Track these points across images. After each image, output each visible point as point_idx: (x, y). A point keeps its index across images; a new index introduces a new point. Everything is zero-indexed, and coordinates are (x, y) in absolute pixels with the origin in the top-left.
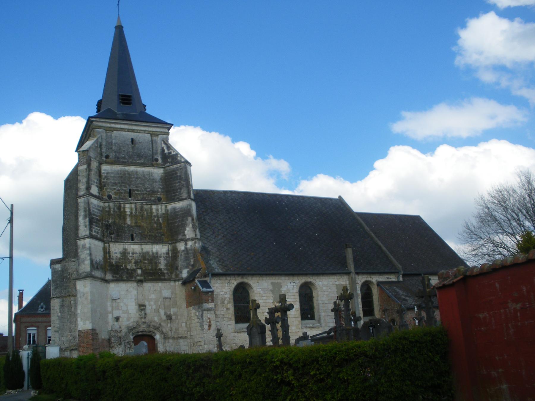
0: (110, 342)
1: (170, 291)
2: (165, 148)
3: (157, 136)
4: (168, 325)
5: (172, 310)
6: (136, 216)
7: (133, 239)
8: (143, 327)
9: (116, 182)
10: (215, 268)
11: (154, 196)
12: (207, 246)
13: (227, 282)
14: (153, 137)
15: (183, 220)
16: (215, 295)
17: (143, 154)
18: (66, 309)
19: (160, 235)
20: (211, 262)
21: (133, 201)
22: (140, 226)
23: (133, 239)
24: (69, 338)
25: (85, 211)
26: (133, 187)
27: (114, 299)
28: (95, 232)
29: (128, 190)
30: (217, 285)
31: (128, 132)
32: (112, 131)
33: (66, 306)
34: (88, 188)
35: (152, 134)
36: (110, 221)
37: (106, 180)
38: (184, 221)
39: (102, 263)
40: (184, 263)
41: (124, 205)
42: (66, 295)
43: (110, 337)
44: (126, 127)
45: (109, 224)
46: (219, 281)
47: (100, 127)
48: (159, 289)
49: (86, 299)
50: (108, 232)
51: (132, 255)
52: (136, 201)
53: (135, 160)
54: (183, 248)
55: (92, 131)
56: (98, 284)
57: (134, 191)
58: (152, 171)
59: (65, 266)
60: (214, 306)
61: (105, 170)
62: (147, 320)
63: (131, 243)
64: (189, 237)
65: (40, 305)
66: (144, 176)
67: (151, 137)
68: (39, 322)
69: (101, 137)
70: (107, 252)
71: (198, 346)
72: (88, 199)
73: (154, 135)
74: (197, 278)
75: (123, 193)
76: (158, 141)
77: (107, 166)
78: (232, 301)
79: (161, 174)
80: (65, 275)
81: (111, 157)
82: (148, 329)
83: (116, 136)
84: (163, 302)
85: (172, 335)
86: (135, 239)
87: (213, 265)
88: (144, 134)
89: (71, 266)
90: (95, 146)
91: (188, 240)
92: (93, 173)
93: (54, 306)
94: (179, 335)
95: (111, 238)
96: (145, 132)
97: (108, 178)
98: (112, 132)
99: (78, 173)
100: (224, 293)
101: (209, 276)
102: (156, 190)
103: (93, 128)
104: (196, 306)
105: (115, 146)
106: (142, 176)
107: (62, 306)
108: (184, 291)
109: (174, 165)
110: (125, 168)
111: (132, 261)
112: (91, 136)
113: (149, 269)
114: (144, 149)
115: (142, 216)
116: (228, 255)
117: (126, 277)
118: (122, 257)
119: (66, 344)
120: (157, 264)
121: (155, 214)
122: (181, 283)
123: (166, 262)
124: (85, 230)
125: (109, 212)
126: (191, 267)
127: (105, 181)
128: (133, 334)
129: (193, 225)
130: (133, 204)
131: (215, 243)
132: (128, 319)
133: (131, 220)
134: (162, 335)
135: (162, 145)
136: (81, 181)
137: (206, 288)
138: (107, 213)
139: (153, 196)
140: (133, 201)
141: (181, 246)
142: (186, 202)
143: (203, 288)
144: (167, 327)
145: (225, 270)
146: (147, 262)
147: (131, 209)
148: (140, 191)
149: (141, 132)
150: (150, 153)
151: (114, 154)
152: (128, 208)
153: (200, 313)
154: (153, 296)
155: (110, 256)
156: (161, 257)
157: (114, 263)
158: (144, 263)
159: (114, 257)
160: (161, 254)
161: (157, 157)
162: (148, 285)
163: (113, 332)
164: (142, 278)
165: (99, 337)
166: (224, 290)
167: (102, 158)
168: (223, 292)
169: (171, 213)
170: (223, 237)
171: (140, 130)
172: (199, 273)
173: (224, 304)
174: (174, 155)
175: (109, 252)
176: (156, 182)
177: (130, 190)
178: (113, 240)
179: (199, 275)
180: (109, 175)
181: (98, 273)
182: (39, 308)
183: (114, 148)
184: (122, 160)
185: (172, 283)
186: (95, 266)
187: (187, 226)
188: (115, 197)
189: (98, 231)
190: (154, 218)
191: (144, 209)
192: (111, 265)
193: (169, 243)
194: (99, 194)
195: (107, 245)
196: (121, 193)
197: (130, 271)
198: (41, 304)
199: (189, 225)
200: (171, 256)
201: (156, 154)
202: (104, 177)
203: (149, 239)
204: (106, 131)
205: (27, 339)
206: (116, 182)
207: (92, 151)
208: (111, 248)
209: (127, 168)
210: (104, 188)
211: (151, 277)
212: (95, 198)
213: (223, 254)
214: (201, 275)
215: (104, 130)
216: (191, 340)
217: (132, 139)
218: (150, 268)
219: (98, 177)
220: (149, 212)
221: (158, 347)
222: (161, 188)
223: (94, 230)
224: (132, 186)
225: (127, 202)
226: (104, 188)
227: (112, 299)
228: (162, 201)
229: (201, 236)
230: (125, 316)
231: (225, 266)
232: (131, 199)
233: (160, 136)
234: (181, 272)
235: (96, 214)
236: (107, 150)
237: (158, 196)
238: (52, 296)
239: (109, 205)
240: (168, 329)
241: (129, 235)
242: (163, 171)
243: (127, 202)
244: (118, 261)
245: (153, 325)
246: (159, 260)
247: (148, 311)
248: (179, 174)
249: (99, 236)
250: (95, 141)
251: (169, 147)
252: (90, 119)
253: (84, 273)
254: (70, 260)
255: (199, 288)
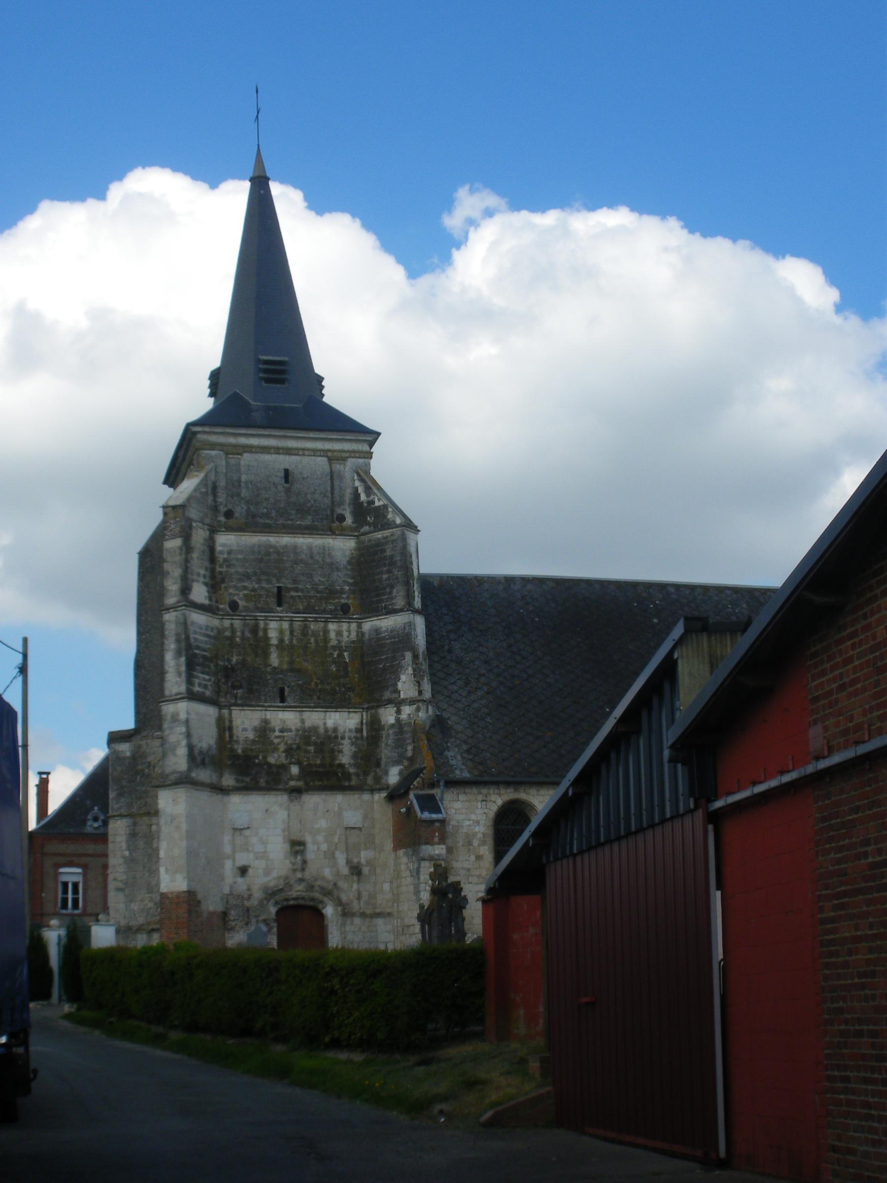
0: (227, 919)
1: (361, 813)
2: (360, 490)
3: (343, 462)
4: (352, 887)
5: (363, 854)
6: (291, 646)
7: (283, 700)
8: (298, 890)
9: (247, 573)
10: (456, 769)
11: (334, 602)
12: (446, 715)
13: (481, 800)
14: (333, 465)
15: (394, 658)
16: (453, 826)
17: (310, 504)
18: (141, 843)
19: (343, 689)
20: (449, 754)
21: (286, 615)
22: (299, 671)
23: (283, 700)
24: (147, 905)
25: (178, 641)
26: (286, 583)
27: (238, 829)
28: (200, 685)
29: (276, 588)
30: (458, 805)
31: (277, 456)
32: (241, 455)
33: (140, 835)
34: (185, 590)
35: (334, 458)
36: (234, 660)
37: (227, 567)
38: (396, 661)
39: (214, 751)
40: (393, 754)
41: (266, 624)
42: (141, 812)
43: (227, 908)
44: (272, 442)
45: (231, 665)
46: (462, 797)
47: (213, 446)
48: (336, 809)
49: (177, 827)
50: (230, 684)
51: (280, 734)
52: (293, 613)
53: (292, 520)
54: (391, 720)
55: (196, 454)
56: (204, 797)
57: (288, 590)
58: (330, 546)
59: (140, 746)
60: (444, 851)
61: (223, 545)
62: (307, 875)
63: (278, 707)
64: (406, 697)
65: (90, 814)
66: (312, 557)
67: (330, 464)
68: (88, 855)
69: (216, 469)
70: (224, 728)
71: (410, 934)
72: (184, 614)
73: (338, 460)
74: (413, 788)
75: (264, 596)
76: (346, 474)
77: (229, 537)
78: (490, 841)
79: (351, 550)
80: (140, 767)
81: (237, 515)
82: (308, 893)
83: (248, 466)
84: (344, 837)
85: (360, 908)
86: (289, 699)
87: (452, 760)
88: (313, 458)
89: (152, 746)
90: (201, 493)
91: (404, 702)
92: (195, 555)
93: (116, 835)
94: (375, 908)
95: (236, 697)
96: (315, 452)
97: (231, 562)
98: (239, 456)
99: (164, 556)
100: (471, 822)
101: (439, 786)
102: (338, 588)
103: (197, 449)
104: (409, 849)
105: (247, 488)
106: (306, 555)
107: (133, 835)
108: (390, 815)
109: (380, 530)
110: (268, 540)
111: (279, 746)
112: (193, 465)
113: (316, 765)
114: (314, 493)
115: (305, 648)
116: (491, 737)
117: (267, 782)
118: (257, 739)
119: (139, 917)
120: (334, 753)
121: (334, 643)
122: (385, 798)
123: (353, 749)
124: (177, 681)
125: (231, 639)
126: (406, 763)
127: (224, 569)
128: (277, 903)
129: (414, 670)
130: (285, 620)
131: (466, 709)
132: (267, 872)
133: (280, 656)
134: (339, 909)
135: (354, 484)
136: (169, 574)
137: (430, 812)
138: (228, 642)
139: (331, 601)
140: (286, 615)
141: (388, 716)
142: (402, 616)
143: (422, 811)
144: (349, 891)
145: (476, 773)
146: (312, 748)
147: (281, 632)
148: (302, 591)
149: (306, 453)
150: (327, 501)
151: (245, 507)
152: (274, 629)
153: (416, 866)
154: (323, 824)
155: (231, 736)
156: (343, 738)
157: (240, 751)
158: (307, 752)
159: (241, 739)
160: (345, 732)
161: (341, 512)
162: (313, 801)
163: (234, 898)
164: (300, 784)
165: (203, 907)
166: (473, 817)
167: (216, 517)
168: (470, 820)
169: (370, 639)
170: (488, 693)
171: (303, 449)
172: (418, 779)
173: (471, 847)
174: (379, 507)
175: (230, 729)
176: (338, 569)
177: (279, 588)
178: (239, 702)
179: (418, 783)
180: (233, 556)
181: (204, 775)
182: (89, 820)
183: (244, 493)
184: (261, 521)
185: (366, 797)
186: (199, 759)
187: (403, 671)
188: (247, 605)
189: (206, 683)
190: (331, 651)
191: (310, 632)
192: (234, 756)
193: (363, 708)
194: (210, 599)
195: (225, 712)
196: (260, 596)
197: (274, 770)
198: (93, 809)
199: (407, 669)
200: (367, 738)
201: (341, 503)
202: (221, 561)
203: (319, 698)
204: (227, 454)
205: (60, 896)
206: (249, 571)
207: (194, 505)
208: (234, 719)
209: (272, 539)
210: (223, 586)
211: (320, 783)
212: (201, 612)
213: (480, 736)
214: (423, 781)
215: (222, 453)
216: (399, 920)
217: (287, 472)
218: (319, 762)
219: (207, 564)
220: (322, 637)
221: (329, 933)
222: (349, 584)
223: (197, 681)
224: (284, 580)
225: (273, 617)
226: (223, 586)
227: (234, 829)
228: (351, 613)
229: (434, 692)
230: (261, 864)
231: (480, 764)
232: (281, 608)
233: (351, 462)
234: (386, 773)
235: (203, 645)
236: (229, 498)
237: (343, 601)
238: (110, 812)
239: (232, 625)
240: (351, 896)
241: (275, 689)
242: (356, 543)
243: (273, 617)
244: (249, 747)
245: (319, 886)
246: (339, 745)
247: (310, 855)
248: (388, 553)
249: (208, 693)
250: (202, 481)
251: (371, 485)
252: (191, 427)
253: (175, 775)
254: (151, 734)
255: (415, 812)
